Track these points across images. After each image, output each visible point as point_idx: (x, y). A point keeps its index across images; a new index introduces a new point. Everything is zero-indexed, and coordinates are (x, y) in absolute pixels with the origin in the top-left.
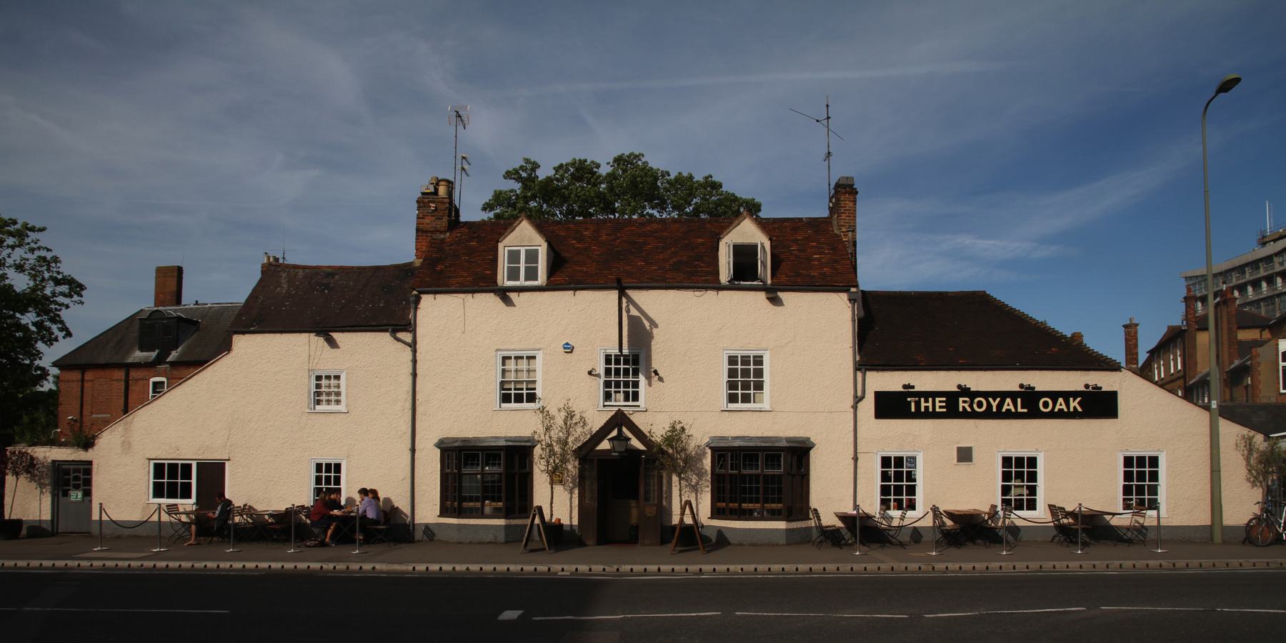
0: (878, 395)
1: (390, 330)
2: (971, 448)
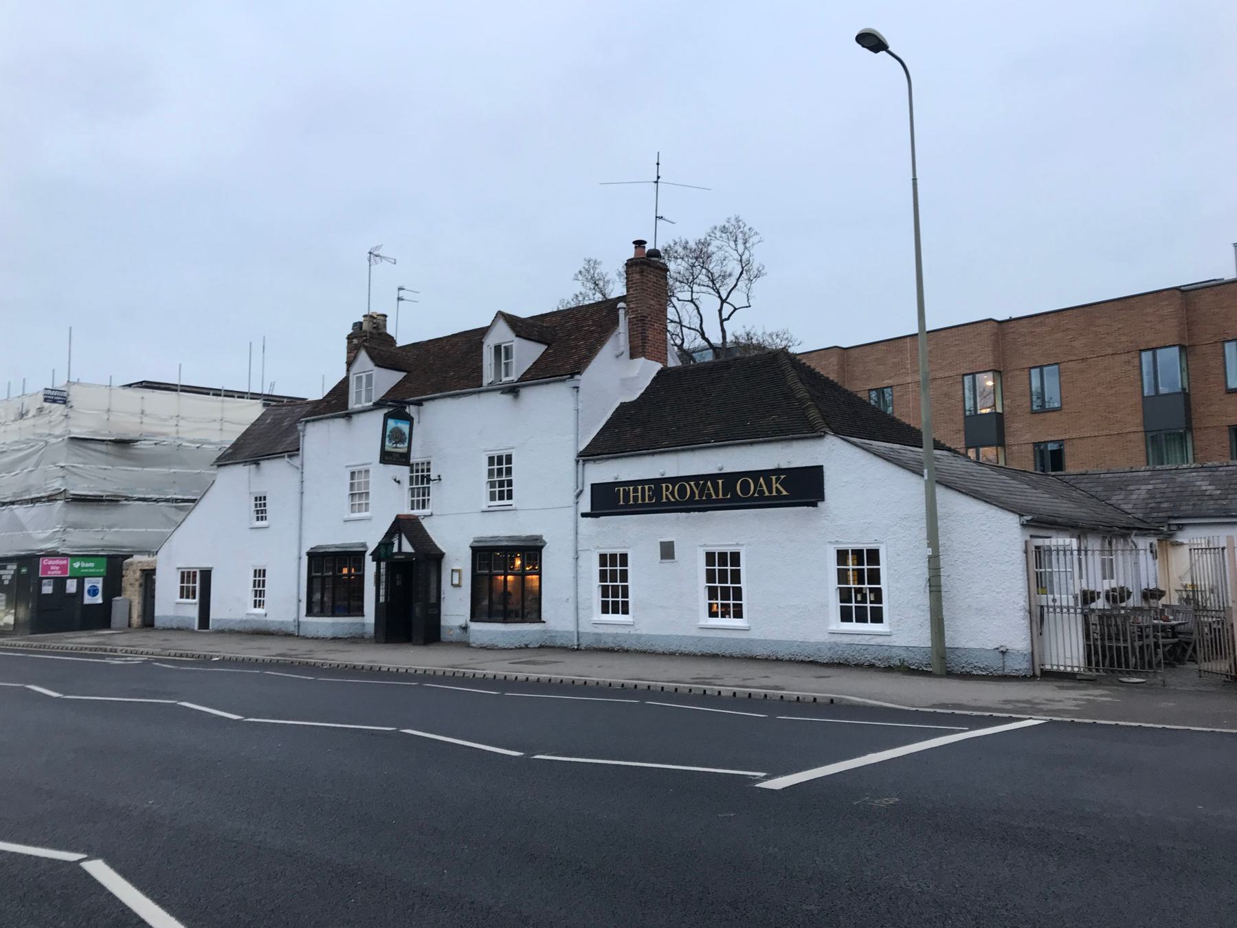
0: (594, 487)
1: (286, 456)
2: (673, 542)
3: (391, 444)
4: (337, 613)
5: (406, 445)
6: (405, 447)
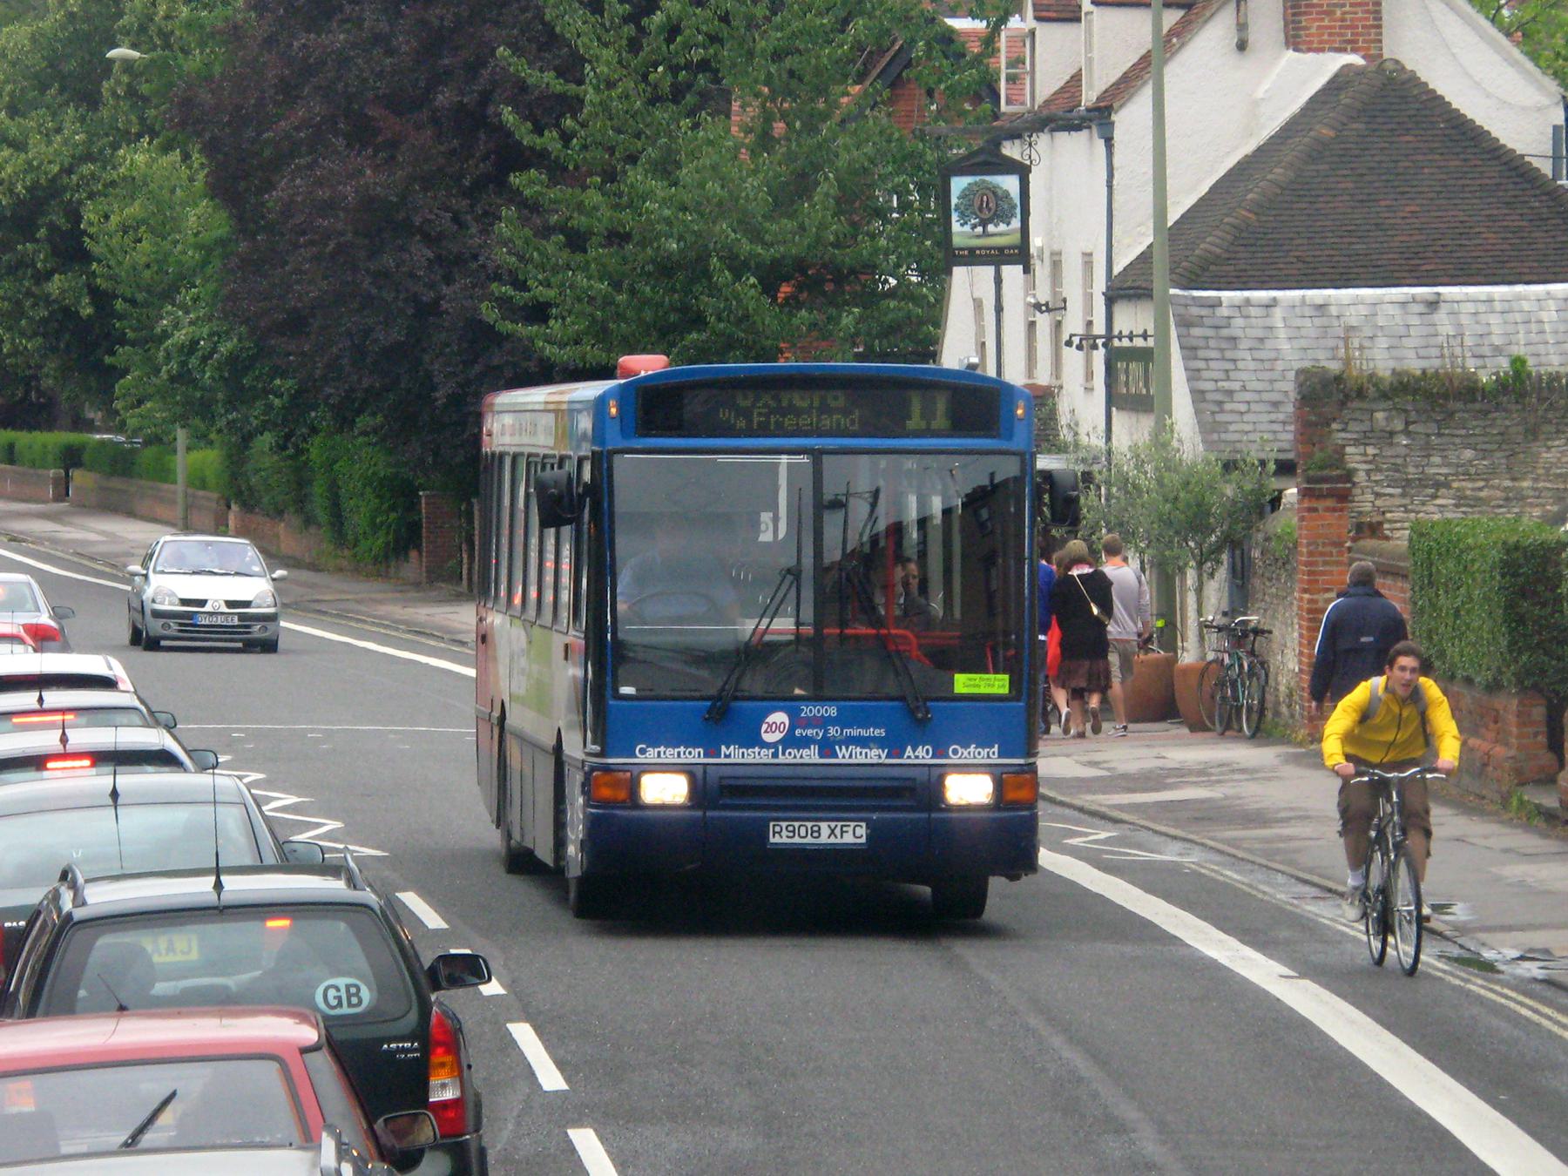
3: (967, 228)
4: (827, 692)
5: (1016, 223)
6: (1013, 231)
